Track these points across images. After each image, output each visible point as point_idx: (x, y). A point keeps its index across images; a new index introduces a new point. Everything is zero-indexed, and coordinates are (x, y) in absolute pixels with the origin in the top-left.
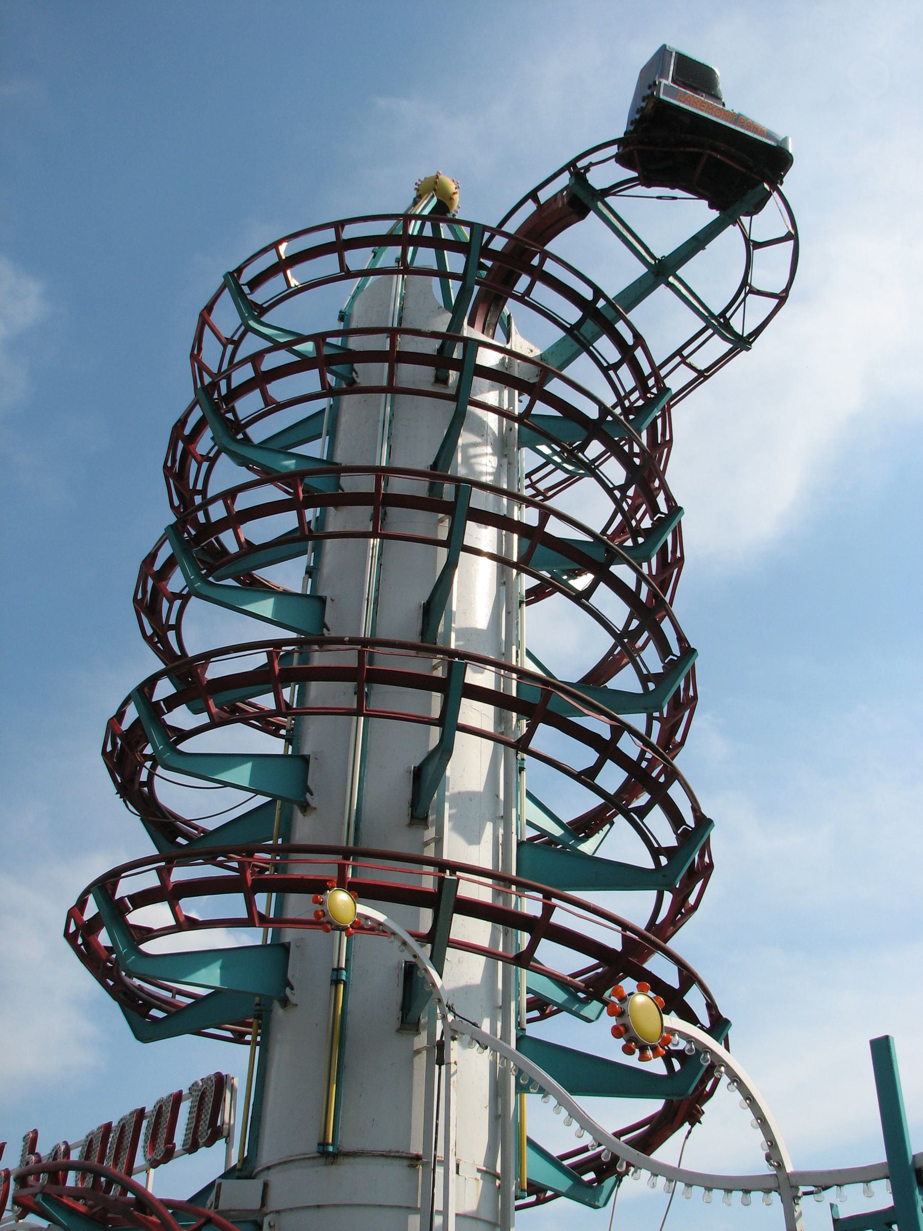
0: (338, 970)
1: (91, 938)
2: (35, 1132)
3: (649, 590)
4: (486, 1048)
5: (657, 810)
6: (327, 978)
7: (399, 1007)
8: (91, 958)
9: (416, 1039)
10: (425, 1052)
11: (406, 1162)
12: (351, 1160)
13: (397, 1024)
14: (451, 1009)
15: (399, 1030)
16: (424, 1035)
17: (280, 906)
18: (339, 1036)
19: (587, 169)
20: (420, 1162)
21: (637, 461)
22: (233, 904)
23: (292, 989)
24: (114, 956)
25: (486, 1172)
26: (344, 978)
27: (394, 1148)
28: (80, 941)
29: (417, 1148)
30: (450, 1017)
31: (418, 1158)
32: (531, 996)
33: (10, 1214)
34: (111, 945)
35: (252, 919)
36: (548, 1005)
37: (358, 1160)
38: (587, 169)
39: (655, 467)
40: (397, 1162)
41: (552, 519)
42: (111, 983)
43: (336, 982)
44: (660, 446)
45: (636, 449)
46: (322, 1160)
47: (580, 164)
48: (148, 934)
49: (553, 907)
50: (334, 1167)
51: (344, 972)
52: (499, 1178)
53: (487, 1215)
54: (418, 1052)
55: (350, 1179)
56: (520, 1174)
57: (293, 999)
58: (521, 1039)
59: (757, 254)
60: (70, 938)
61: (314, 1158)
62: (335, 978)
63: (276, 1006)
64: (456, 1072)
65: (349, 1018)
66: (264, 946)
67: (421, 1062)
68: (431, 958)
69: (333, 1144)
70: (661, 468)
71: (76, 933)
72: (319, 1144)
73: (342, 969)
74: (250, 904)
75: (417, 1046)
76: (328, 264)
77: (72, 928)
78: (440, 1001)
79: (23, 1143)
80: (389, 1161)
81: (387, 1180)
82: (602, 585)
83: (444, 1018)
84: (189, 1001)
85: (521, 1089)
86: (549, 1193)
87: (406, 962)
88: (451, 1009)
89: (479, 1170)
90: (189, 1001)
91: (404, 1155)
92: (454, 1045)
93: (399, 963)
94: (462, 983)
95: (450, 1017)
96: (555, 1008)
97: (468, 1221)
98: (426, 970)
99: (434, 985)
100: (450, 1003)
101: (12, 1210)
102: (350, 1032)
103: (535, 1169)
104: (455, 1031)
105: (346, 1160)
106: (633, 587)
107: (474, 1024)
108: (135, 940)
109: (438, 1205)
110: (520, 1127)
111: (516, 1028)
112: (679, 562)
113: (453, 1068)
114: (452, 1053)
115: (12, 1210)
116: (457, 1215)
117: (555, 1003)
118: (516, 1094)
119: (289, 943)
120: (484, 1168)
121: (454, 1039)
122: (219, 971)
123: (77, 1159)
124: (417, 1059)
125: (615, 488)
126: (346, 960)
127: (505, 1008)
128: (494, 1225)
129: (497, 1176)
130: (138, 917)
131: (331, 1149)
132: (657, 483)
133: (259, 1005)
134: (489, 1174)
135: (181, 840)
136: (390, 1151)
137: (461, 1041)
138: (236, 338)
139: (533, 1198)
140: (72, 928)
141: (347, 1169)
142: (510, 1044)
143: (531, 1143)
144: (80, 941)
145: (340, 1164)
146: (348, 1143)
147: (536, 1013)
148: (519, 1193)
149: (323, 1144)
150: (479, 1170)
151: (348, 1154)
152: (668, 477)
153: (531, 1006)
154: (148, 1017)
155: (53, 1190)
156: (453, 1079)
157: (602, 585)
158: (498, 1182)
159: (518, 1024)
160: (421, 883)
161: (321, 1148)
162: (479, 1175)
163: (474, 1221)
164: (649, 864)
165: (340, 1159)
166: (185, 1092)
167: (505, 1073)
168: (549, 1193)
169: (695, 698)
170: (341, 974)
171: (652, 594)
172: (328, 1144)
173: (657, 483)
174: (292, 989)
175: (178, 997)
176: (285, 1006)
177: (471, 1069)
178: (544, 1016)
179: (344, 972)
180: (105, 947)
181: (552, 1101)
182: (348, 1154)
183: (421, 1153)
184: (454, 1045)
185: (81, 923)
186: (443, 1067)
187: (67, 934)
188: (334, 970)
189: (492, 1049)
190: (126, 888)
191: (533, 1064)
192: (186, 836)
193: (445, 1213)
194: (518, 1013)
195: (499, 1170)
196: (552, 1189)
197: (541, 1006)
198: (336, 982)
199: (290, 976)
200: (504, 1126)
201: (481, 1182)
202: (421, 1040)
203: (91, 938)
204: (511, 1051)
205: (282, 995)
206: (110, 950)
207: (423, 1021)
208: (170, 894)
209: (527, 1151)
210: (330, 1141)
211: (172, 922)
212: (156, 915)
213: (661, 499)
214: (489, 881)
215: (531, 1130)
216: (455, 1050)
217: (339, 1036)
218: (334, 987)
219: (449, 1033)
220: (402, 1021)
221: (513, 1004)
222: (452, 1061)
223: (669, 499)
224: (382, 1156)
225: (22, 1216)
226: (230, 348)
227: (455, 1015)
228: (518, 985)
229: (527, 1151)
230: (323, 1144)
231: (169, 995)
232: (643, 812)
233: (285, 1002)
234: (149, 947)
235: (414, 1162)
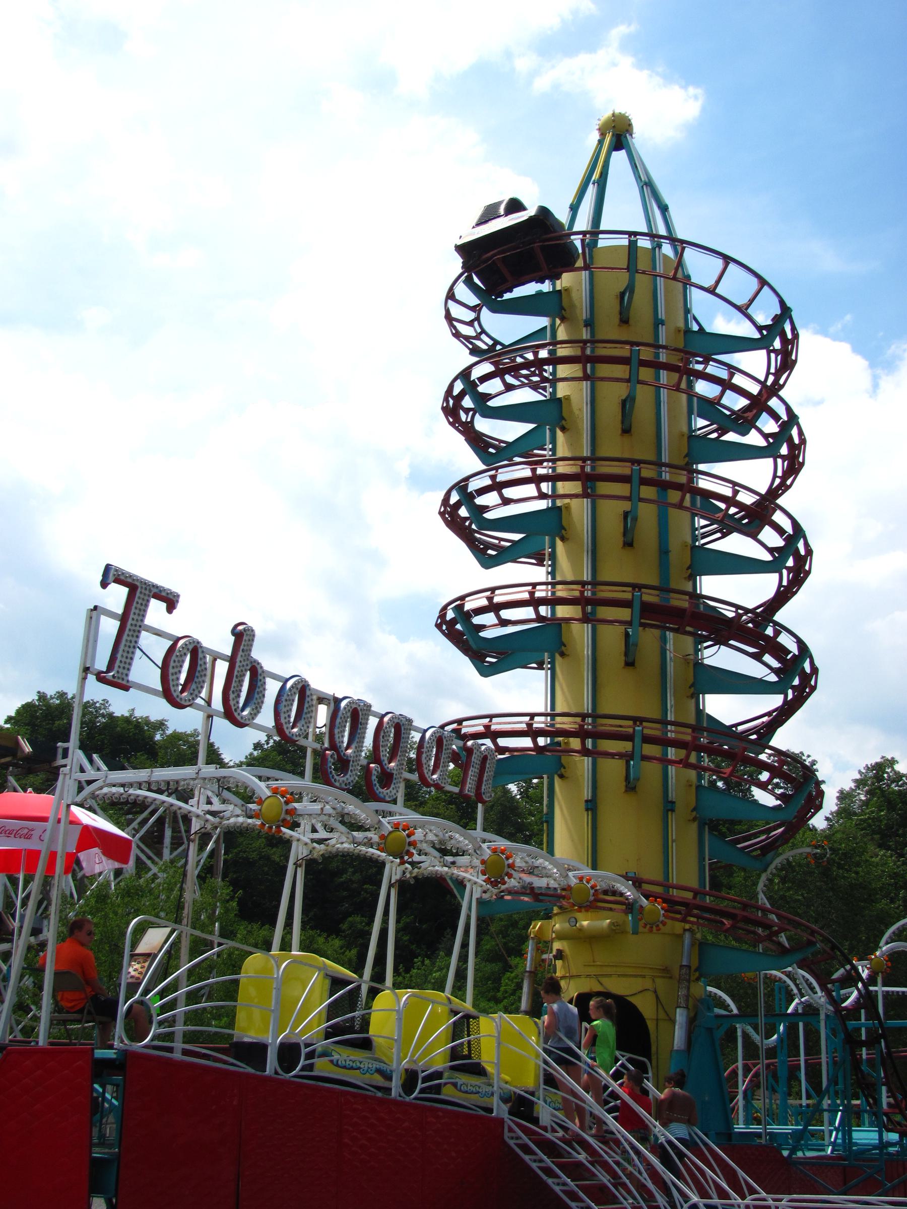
17: (554, 488)
22: (530, 490)
35: (542, 496)
49: (738, 491)
60: (442, 514)
74: (539, 489)
82: (771, 744)
84: (508, 544)
90: (508, 544)
130: (480, 501)
135: (491, 450)
154: (488, 556)
157: (771, 744)
164: (764, 444)
166: (200, 730)
175: (502, 543)
190: (473, 485)
191: (453, 887)
192: (494, 446)
208: (497, 486)
212: (491, 499)
214: (652, 467)
223: (806, 545)
231: (497, 542)
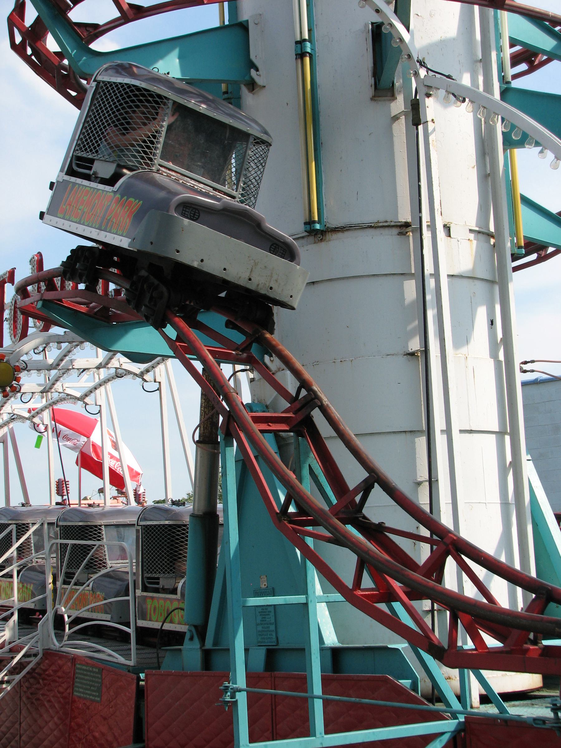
0: (301, 42)
1: (38, 45)
2: (40, 254)
4: (464, 101)
6: (291, 51)
7: (370, 74)
8: (45, 67)
9: (393, 105)
10: (403, 117)
11: (395, 231)
12: (340, 235)
13: (370, 92)
14: (422, 64)
15: (373, 98)
16: (400, 99)
18: (312, 114)
20: (409, 229)
23: (257, 70)
24: (66, 62)
25: (479, 232)
26: (309, 50)
27: (382, 219)
28: (29, 51)
29: (405, 215)
30: (423, 72)
31: (407, 225)
32: (518, 48)
33: (34, 330)
34: (60, 50)
36: (536, 55)
37: (346, 234)
40: (386, 231)
42: (74, 94)
43: (301, 56)
46: (311, 239)
48: (95, 31)
50: (323, 244)
51: (308, 44)
52: (493, 237)
53: (483, 273)
54: (396, 118)
55: (342, 252)
56: (515, 232)
57: (260, 81)
58: (506, 92)
61: (303, 237)
62: (299, 52)
63: (244, 90)
64: (434, 130)
65: (320, 93)
66: (223, 28)
67: (400, 128)
68: (396, 12)
69: (319, 222)
71: (23, 43)
72: (306, 223)
73: (305, 40)
75: (394, 112)
77: (18, 39)
78: (409, 56)
79: (30, 267)
80: (378, 231)
81: (380, 250)
83: (416, 74)
85: (509, 143)
86: (551, 250)
87: (372, 24)
88: (422, 64)
89: (471, 231)
91: (393, 224)
92: (429, 102)
93: (366, 25)
94: (436, 38)
95: (423, 72)
96: (545, 57)
97: (465, 282)
98: (391, 25)
99: (401, 40)
100: (420, 58)
101: (35, 326)
102: (323, 107)
103: (531, 226)
104: (429, 87)
105: (335, 236)
107: (449, 77)
108: (82, 39)
109: (429, 268)
110: (511, 186)
111: (499, 81)
113: (431, 126)
114: (428, 110)
115: (35, 326)
116: (450, 276)
117: (544, 52)
118: (505, 150)
119: (247, 21)
120: (477, 229)
121: (428, 95)
122: (178, 60)
123: (417, 440)
124: (395, 126)
126: (310, 31)
127: (485, 61)
128: (492, 282)
129: (492, 236)
131: (318, 226)
133: (226, 93)
134: (482, 233)
136: (378, 222)
137: (437, 97)
139: (534, 257)
140: (18, 39)
141: (336, 244)
142: (493, 94)
143: (526, 201)
144: (29, 51)
145: (329, 240)
146: (334, 219)
147: (523, 67)
148: (516, 251)
149: (310, 223)
150: (471, 231)
151: (336, 230)
153: (516, 60)
155: (51, 295)
156: (431, 138)
158: (492, 241)
159: (503, 79)
160: (461, 6)
161: (308, 226)
162: (472, 236)
163: (471, 280)
165: (329, 236)
167: (491, 130)
168: (551, 250)
170: (305, 47)
172: (314, 222)
174: (257, 70)
176: (253, 90)
177: (452, 129)
178: (532, 68)
179: (308, 44)
180: (55, 53)
181: (550, 155)
182: (336, 230)
183: (409, 220)
184: (429, 102)
185: (24, 31)
186: (420, 127)
187: (13, 46)
188: (297, 43)
189: (471, 101)
193: (436, 275)
194: (501, 68)
195: (492, 229)
196: (553, 245)
197: (529, 57)
198: (301, 56)
199: (252, 57)
200: (495, 185)
201: (475, 242)
202: (399, 105)
203: (38, 45)
204: (480, 94)
205: (247, 78)
206: (60, 55)
207: (397, 84)
209: (522, 209)
210: (316, 219)
211: (117, 14)
215: (524, 188)
216: (432, 107)
217: (312, 114)
218: (299, 61)
219: (423, 90)
220: (376, 88)
221: (494, 55)
222: (429, 119)
224: (371, 227)
225: (46, 329)
227: (428, 69)
228: (499, 36)
229: (522, 209)
230: (310, 223)
233: (252, 85)
234: (101, 45)
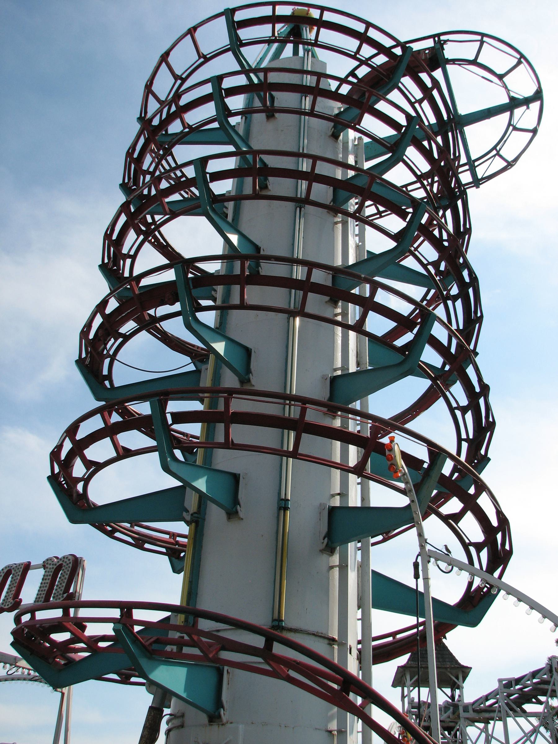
3: (457, 343)
5: (469, 515)
11: (326, 641)
19: (445, 41)
21: (446, 244)
38: (445, 41)
39: (460, 250)
40: (321, 640)
41: (380, 290)
44: (462, 233)
45: (445, 236)
47: (442, 38)
54: (332, 567)
59: (479, 61)
70: (464, 250)
73: (288, 500)
76: (351, 44)
80: (317, 639)
106: (445, 343)
112: (480, 320)
125: (429, 263)
132: (461, 260)
138: (184, 76)
152: (469, 256)
169: (482, 316)
171: (459, 346)
172: (282, 621)
173: (461, 260)
213: (465, 273)
224: (314, 634)
226: (179, 82)
232: (458, 517)
235: (331, 642)
